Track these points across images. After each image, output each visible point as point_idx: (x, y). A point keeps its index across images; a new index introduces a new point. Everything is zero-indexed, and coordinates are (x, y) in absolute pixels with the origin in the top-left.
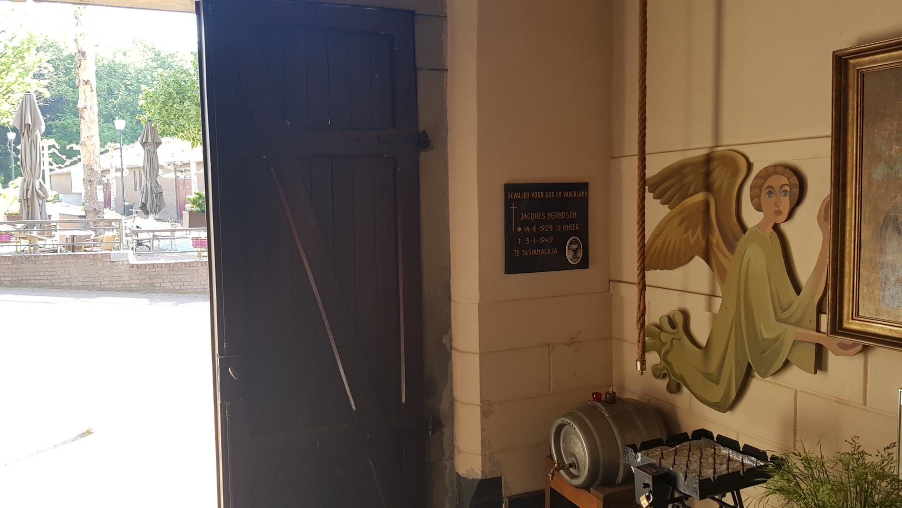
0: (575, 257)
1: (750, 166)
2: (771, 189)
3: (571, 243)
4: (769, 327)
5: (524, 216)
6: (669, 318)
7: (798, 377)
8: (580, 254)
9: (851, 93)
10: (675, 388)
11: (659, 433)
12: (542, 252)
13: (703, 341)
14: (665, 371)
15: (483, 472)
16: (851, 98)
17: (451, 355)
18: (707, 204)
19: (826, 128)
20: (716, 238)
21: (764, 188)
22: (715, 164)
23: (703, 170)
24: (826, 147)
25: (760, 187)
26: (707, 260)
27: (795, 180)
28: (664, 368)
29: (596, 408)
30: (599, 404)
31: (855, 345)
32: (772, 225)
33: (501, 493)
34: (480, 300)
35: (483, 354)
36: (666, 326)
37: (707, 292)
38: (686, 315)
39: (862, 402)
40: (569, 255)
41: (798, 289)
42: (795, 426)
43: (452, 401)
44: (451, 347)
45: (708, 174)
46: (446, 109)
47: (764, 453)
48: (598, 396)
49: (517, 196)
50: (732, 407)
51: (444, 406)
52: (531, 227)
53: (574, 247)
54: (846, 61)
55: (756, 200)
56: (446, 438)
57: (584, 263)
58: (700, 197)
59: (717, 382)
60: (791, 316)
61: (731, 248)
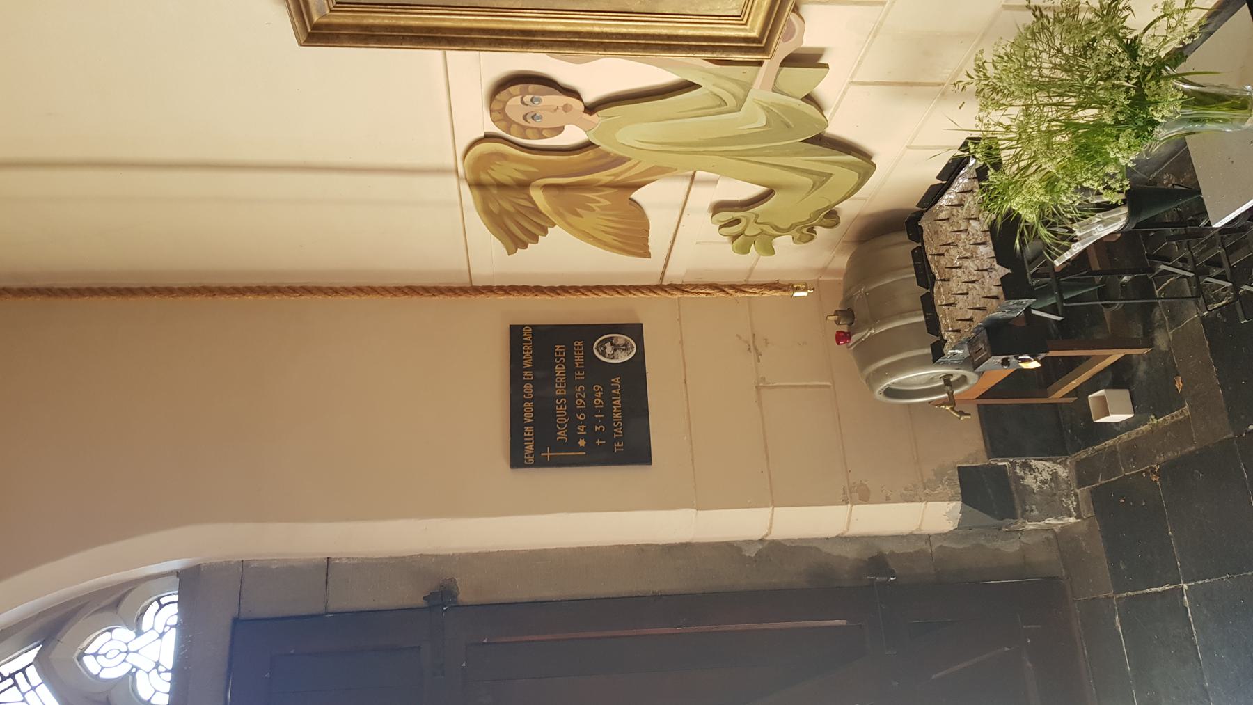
0: (625, 348)
1: (489, 137)
2: (528, 117)
3: (603, 354)
4: (752, 118)
5: (562, 435)
6: (721, 227)
7: (827, 87)
8: (621, 339)
9: (370, 21)
10: (831, 216)
11: (902, 249)
12: (617, 402)
13: (760, 190)
14: (805, 231)
15: (951, 499)
16: (377, 22)
17: (773, 542)
18: (546, 187)
19: (432, 57)
20: (603, 177)
21: (524, 123)
22: (484, 177)
23: (495, 191)
24: (461, 59)
25: (525, 128)
26: (637, 186)
27: (516, 89)
28: (799, 231)
29: (861, 344)
30: (855, 338)
31: (789, 23)
32: (586, 116)
33: (982, 467)
34: (691, 507)
35: (776, 502)
36: (736, 229)
37: (687, 183)
38: (718, 207)
39: (880, 8)
40: (623, 358)
41: (688, 86)
42: (906, 84)
43: (842, 539)
44: (762, 540)
45: (501, 186)
46: (391, 558)
47: (954, 159)
48: (842, 337)
49: (529, 448)
50: (865, 155)
51: (850, 552)
52: (579, 423)
53: (609, 348)
54: (316, 27)
55: (544, 133)
56: (899, 548)
57: (635, 331)
58: (538, 196)
59: (829, 175)
60: (734, 95)
61: (620, 160)
